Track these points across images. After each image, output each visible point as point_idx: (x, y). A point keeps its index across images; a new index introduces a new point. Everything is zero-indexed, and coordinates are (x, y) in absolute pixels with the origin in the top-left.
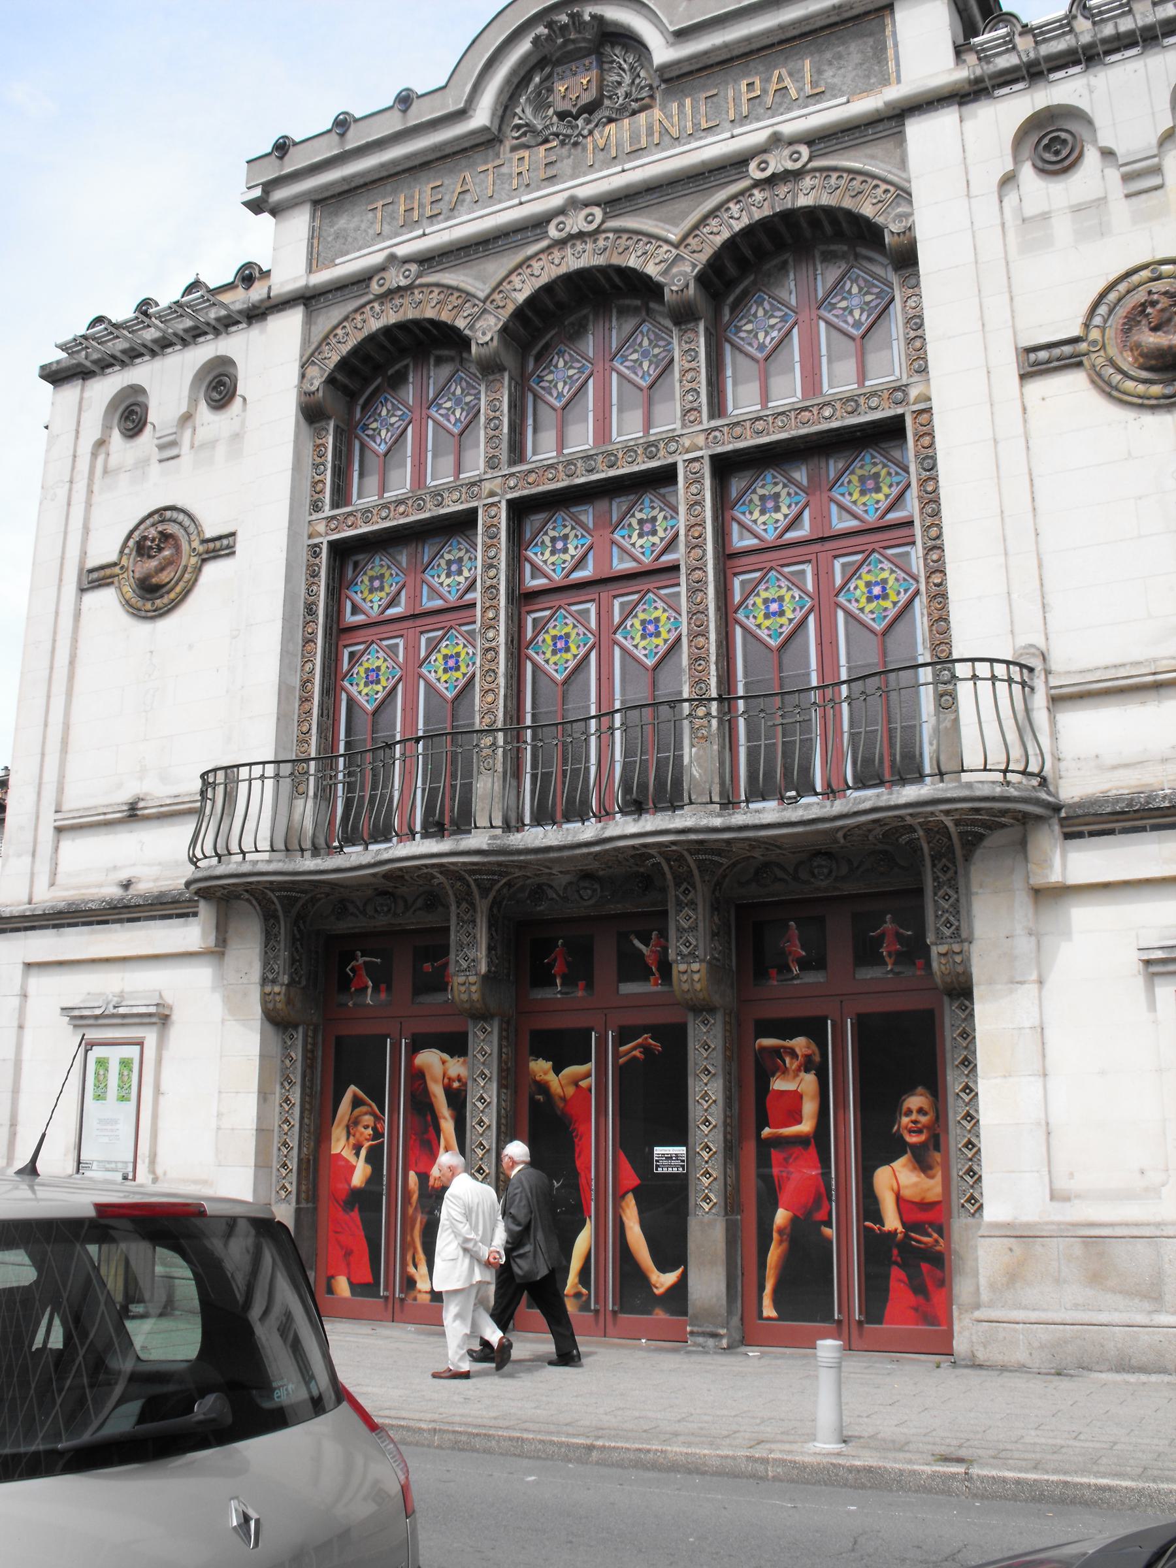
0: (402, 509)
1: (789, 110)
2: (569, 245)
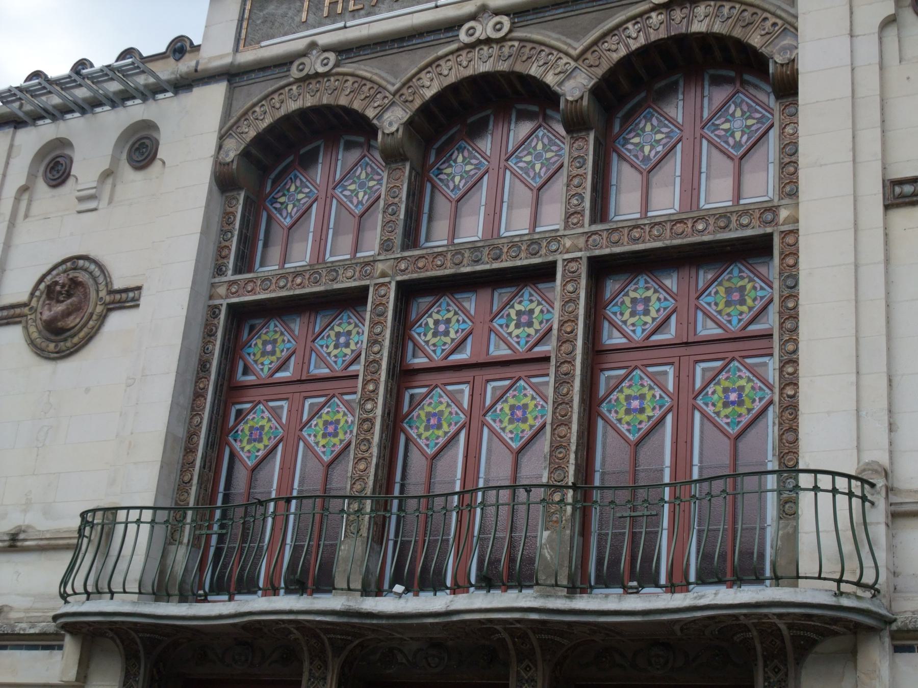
2: (477, 49)
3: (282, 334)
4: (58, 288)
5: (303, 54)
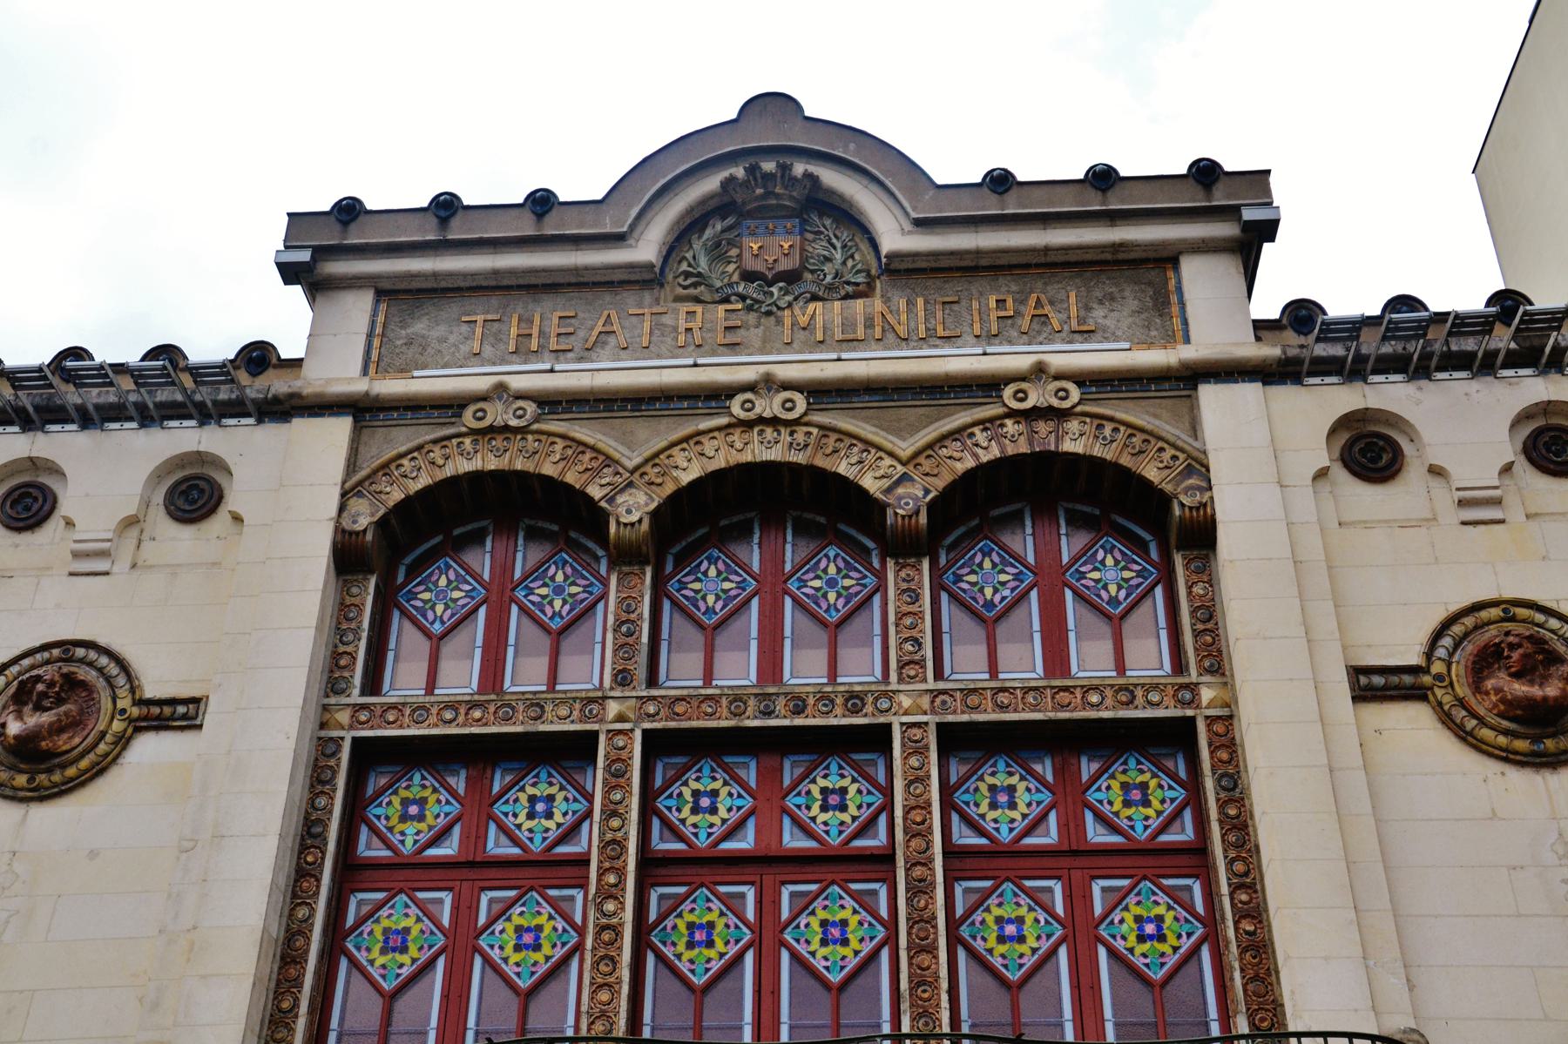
0: (477, 714)
1: (1050, 341)
2: (756, 430)
3: (435, 790)
4: (40, 687)
5: (483, 398)
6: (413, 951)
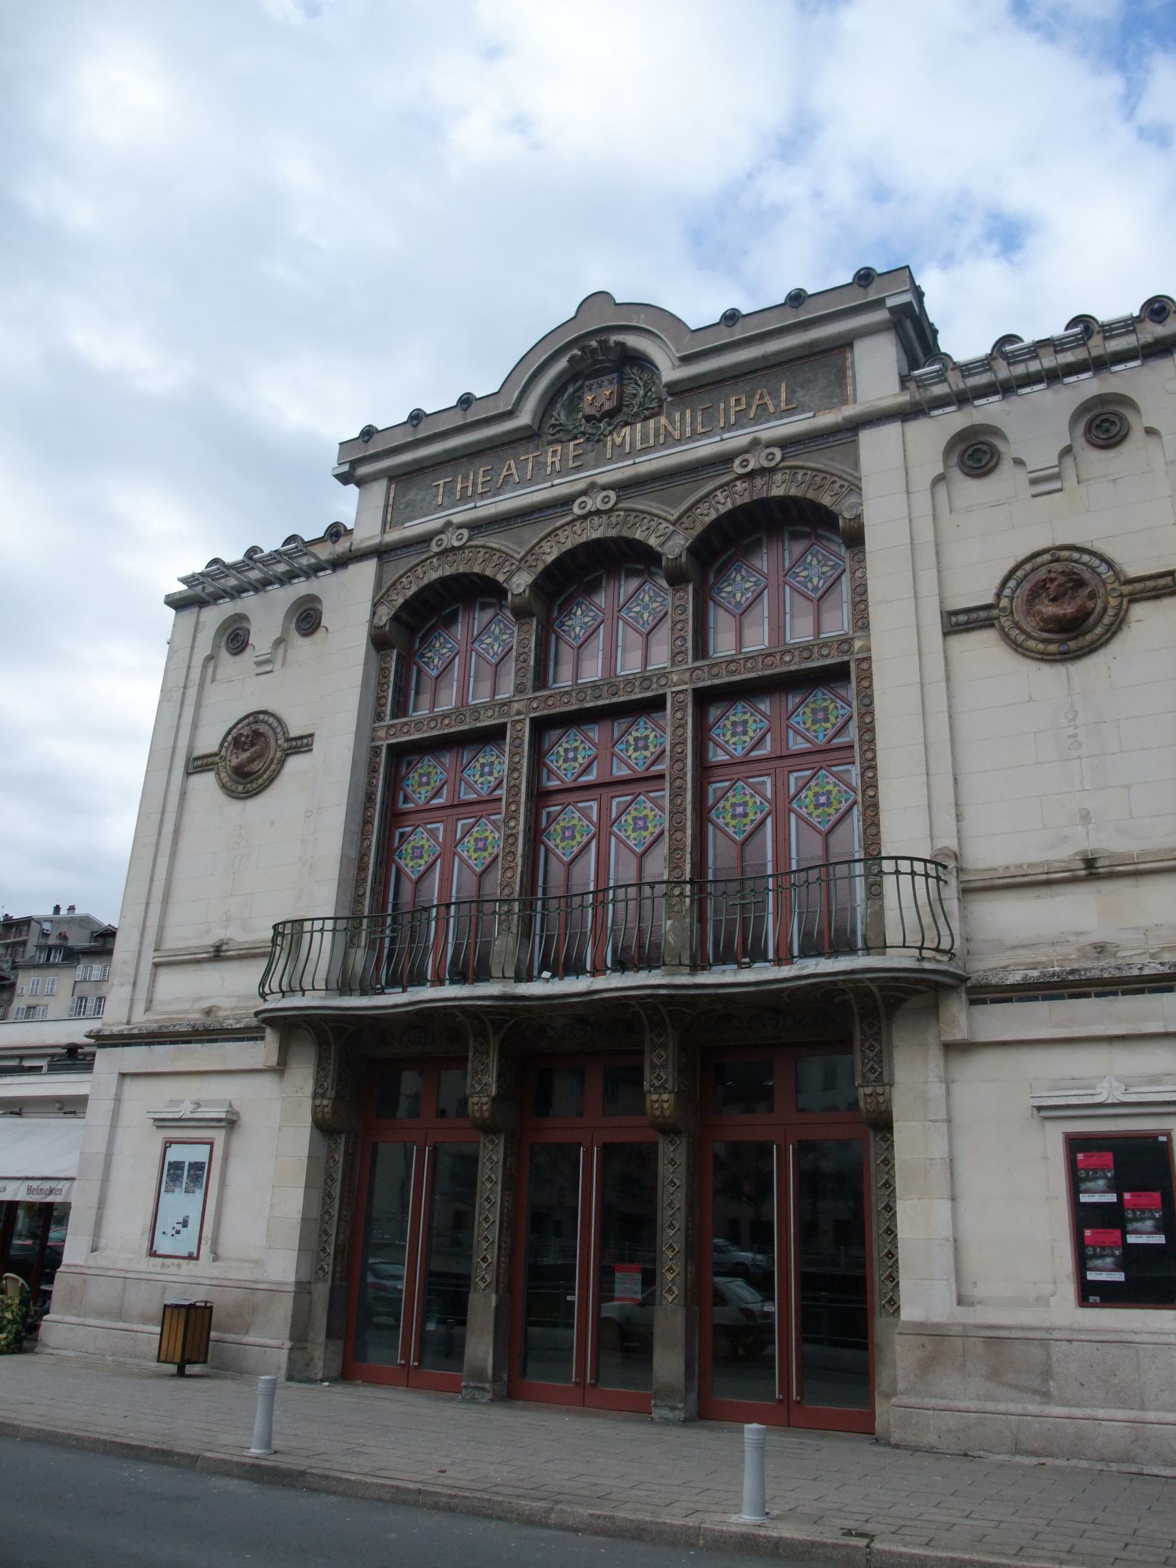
1: (768, 421)
4: (243, 739)
6: (426, 858)
